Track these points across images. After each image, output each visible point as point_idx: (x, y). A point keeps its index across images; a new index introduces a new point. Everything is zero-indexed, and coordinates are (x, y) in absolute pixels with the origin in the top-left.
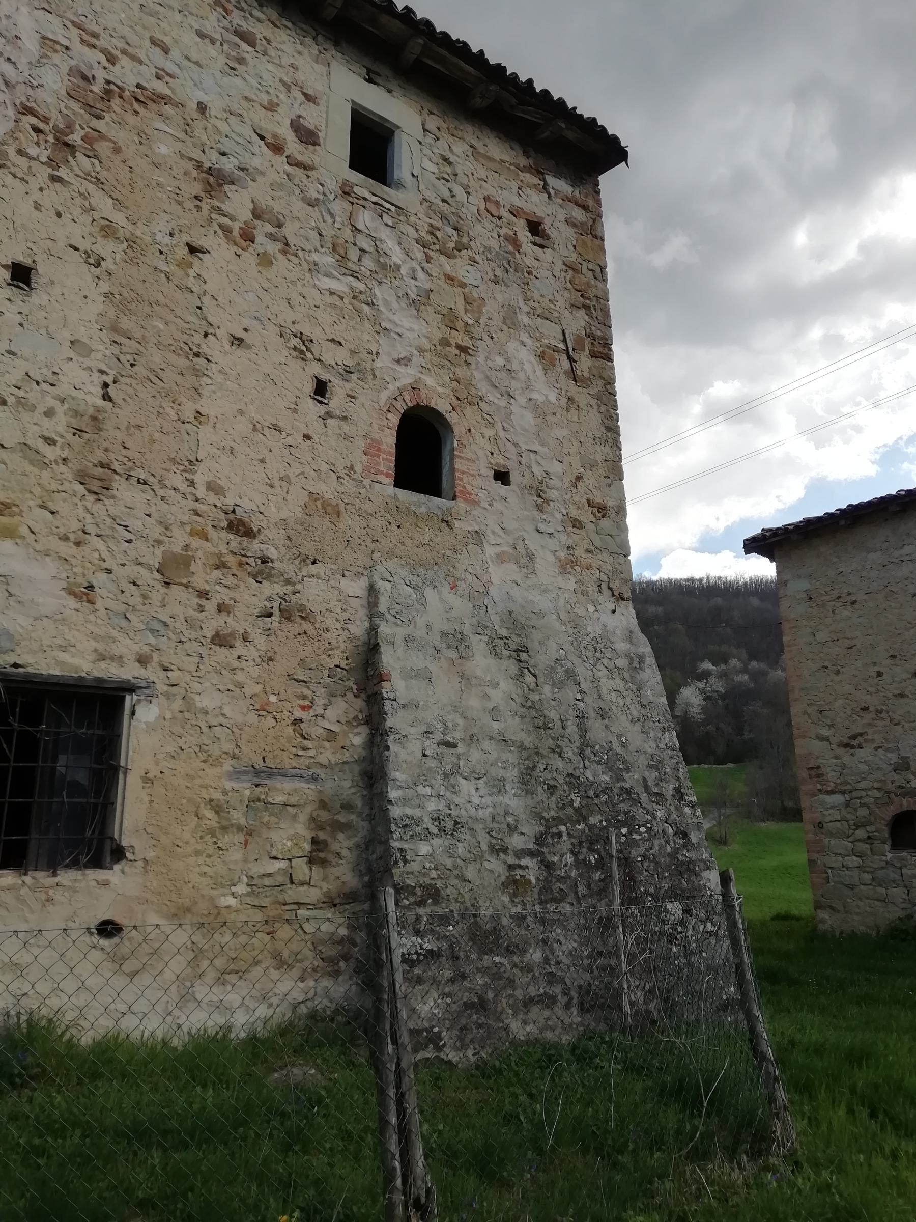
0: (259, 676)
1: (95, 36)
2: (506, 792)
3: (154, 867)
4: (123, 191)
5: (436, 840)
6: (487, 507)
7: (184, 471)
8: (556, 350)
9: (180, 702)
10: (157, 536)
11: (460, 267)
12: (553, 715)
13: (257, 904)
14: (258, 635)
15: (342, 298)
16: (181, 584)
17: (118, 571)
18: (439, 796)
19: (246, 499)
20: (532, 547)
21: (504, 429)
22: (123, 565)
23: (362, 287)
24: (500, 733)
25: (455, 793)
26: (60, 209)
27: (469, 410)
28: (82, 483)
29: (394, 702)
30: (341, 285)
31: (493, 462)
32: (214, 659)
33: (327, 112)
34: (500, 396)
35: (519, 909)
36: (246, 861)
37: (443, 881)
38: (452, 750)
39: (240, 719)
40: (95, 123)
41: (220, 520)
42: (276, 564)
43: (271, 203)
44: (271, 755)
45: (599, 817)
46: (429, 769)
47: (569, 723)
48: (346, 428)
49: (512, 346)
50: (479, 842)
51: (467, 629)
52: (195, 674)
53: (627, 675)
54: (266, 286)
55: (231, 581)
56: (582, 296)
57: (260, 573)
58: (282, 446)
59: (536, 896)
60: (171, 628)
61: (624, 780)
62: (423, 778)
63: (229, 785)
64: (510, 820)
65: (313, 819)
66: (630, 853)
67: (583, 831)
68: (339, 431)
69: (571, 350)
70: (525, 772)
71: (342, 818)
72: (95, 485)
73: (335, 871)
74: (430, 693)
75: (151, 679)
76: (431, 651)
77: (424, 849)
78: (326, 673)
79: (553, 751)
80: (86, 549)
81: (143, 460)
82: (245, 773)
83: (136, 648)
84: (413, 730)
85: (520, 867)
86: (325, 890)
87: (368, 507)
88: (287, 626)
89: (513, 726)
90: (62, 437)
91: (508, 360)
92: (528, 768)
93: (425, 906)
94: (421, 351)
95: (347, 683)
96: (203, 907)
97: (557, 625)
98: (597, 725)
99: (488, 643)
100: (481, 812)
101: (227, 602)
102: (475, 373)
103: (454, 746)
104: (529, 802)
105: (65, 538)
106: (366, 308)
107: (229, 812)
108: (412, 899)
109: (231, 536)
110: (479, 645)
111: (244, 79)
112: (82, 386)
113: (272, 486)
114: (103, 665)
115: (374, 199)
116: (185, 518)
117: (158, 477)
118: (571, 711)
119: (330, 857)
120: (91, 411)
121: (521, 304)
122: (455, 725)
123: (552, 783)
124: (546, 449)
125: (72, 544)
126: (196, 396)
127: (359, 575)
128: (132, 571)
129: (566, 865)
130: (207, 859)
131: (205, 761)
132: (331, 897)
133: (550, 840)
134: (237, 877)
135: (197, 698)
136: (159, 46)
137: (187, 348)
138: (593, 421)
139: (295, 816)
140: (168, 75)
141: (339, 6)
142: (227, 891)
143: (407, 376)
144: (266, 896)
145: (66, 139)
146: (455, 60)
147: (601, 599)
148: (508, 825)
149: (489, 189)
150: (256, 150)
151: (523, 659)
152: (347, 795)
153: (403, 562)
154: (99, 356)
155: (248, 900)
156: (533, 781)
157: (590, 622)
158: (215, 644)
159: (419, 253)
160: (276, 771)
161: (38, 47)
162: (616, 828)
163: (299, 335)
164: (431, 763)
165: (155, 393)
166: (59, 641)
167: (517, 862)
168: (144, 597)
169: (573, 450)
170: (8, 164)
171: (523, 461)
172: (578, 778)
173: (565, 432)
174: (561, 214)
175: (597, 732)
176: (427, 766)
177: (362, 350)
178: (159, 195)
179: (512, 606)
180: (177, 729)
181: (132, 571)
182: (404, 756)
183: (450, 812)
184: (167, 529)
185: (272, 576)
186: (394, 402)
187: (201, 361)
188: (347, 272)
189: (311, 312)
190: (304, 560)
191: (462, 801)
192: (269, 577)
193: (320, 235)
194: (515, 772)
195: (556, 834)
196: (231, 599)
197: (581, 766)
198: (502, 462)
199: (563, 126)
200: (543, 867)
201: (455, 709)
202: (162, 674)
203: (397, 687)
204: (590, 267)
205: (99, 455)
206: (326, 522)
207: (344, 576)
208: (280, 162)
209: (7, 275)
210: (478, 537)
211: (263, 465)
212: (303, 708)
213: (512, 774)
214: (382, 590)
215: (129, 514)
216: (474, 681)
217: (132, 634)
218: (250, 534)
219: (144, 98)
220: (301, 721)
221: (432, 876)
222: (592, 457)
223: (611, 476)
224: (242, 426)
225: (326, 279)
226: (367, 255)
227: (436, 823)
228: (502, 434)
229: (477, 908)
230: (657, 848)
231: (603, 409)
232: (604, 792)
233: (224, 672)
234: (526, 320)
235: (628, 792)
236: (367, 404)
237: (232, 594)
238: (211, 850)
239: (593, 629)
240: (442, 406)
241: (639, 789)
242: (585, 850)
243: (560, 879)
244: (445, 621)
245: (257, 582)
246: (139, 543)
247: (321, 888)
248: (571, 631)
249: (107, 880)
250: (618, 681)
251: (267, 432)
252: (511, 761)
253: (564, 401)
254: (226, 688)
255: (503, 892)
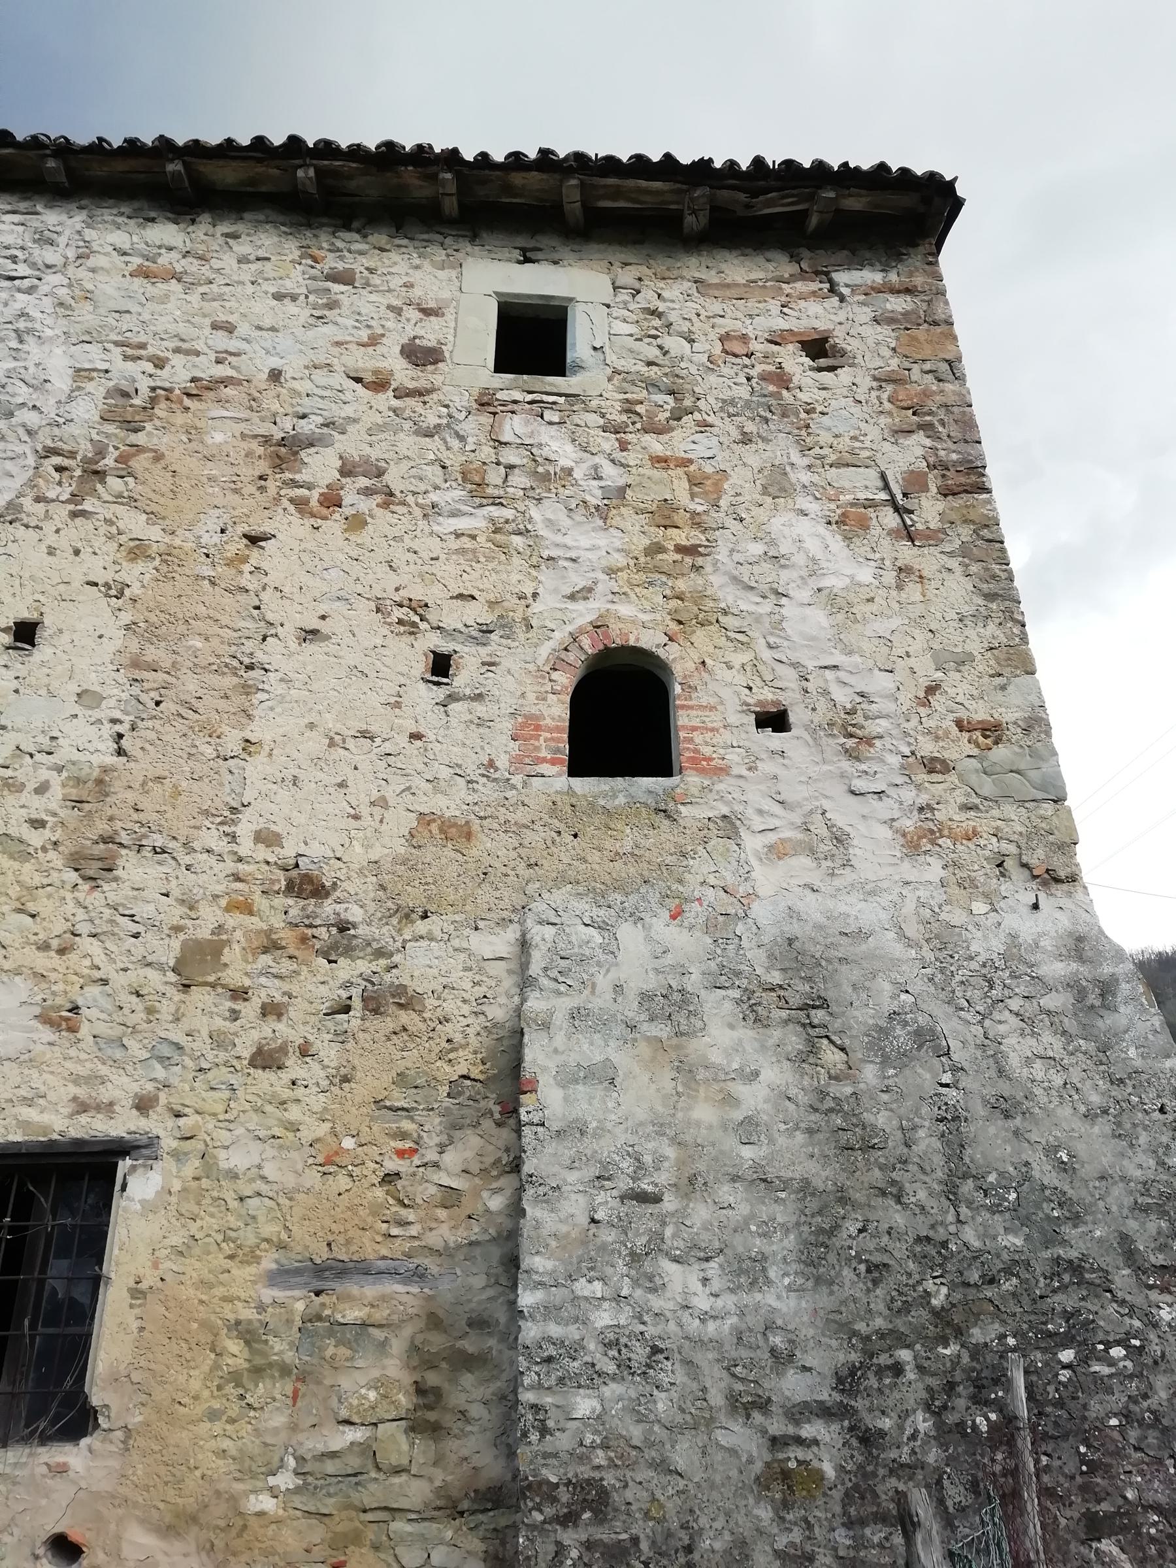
0: (325, 1109)
1: (142, 346)
2: (769, 1282)
3: (141, 1442)
4: (162, 501)
5: (613, 1386)
6: (745, 773)
7: (221, 823)
8: (871, 504)
9: (197, 1163)
10: (175, 921)
11: (683, 441)
12: (881, 1120)
13: (313, 1509)
14: (326, 1043)
15: (474, 537)
16: (206, 984)
17: (119, 981)
18: (618, 1298)
19: (315, 845)
20: (840, 820)
21: (770, 647)
22: (125, 970)
23: (508, 513)
24: (756, 1166)
25: (653, 1290)
26: (79, 545)
27: (700, 636)
28: (76, 870)
29: (540, 1129)
30: (477, 521)
31: (750, 701)
32: (253, 1089)
33: (456, 320)
34: (759, 600)
35: (796, 1535)
36: (294, 1428)
37: (620, 1473)
38: (651, 1208)
39: (290, 1181)
40: (134, 438)
41: (273, 882)
42: (362, 930)
43: (368, 450)
44: (341, 1239)
45: (996, 1328)
46: (603, 1248)
47: (921, 1133)
48: (480, 709)
49: (777, 524)
50: (704, 1390)
51: (694, 982)
52: (221, 1117)
53: (1070, 1024)
54: (354, 554)
55: (286, 966)
56: (914, 414)
57: (334, 947)
58: (375, 758)
59: (838, 1509)
60: (188, 1050)
61: (1064, 1243)
62: (589, 1264)
63: (268, 1294)
64: (777, 1340)
65: (414, 1349)
66: (1085, 1407)
67: (956, 1360)
68: (470, 717)
69: (899, 497)
70: (812, 1239)
71: (470, 1345)
72: (92, 869)
73: (455, 1447)
74: (611, 1105)
75: (155, 1132)
76: (618, 1030)
77: (585, 1405)
78: (444, 1090)
79: (883, 1193)
80: (73, 957)
81: (163, 822)
82: (297, 1272)
83: (135, 1088)
84: (572, 1177)
85: (800, 1441)
86: (438, 1483)
87: (521, 816)
88: (375, 1023)
89: (796, 1155)
90: (55, 814)
91: (773, 543)
92: (821, 1231)
93: (576, 1525)
94: (611, 572)
95: (483, 1104)
96: (218, 1513)
97: (899, 950)
98: (992, 1130)
99: (739, 1002)
100: (711, 1326)
101: (278, 998)
102: (712, 578)
103: (656, 1199)
104: (824, 1300)
105: (44, 947)
106: (517, 540)
107: (266, 1341)
108: (549, 1511)
109: (291, 901)
110: (718, 1010)
111: (336, 324)
112: (87, 746)
113: (356, 817)
114: (84, 1119)
115: (530, 397)
116: (219, 889)
117: (182, 839)
118: (925, 1110)
119: (448, 1420)
120: (96, 773)
121: (795, 457)
122: (659, 1160)
123: (877, 1258)
124: (856, 658)
125: (53, 954)
126: (244, 720)
127: (504, 922)
128: (137, 975)
129: (913, 1437)
130: (228, 1427)
131: (231, 1257)
132: (449, 1497)
133: (873, 1382)
134: (276, 1459)
135: (222, 1154)
136: (221, 328)
137: (235, 663)
138: (956, 591)
139: (383, 1345)
140: (231, 354)
141: (454, 191)
142: (260, 1484)
143: (584, 613)
144: (329, 1495)
145: (95, 467)
146: (631, 183)
147: (1005, 887)
148: (773, 1351)
149: (727, 325)
150: (348, 396)
151: (816, 1021)
152: (480, 1303)
153: (581, 889)
154: (112, 702)
155: (297, 1501)
156: (832, 1258)
157: (979, 934)
158: (255, 1067)
159: (608, 443)
160: (352, 1265)
161: (70, 382)
162: (1044, 1350)
163: (406, 602)
164: (608, 1236)
165: (185, 730)
166: (23, 1092)
167: (791, 1430)
168: (150, 1011)
169: (916, 647)
170: (23, 516)
171: (810, 686)
172: (944, 1244)
173: (895, 622)
174: (864, 314)
175: (991, 1144)
176: (598, 1241)
177: (508, 596)
178: (210, 490)
179: (795, 929)
180: (190, 1207)
181: (137, 975)
182: (555, 1220)
183: (642, 1328)
184: (191, 908)
185: (353, 949)
186: (563, 655)
187: (256, 674)
188: (485, 501)
189: (426, 568)
190: (407, 916)
191: (671, 1305)
192: (348, 951)
193: (444, 467)
194: (791, 1240)
195: (888, 1367)
196: (284, 993)
197: (951, 1218)
198: (770, 697)
199: (832, 195)
200: (855, 1443)
201: (661, 1128)
202: (171, 1122)
203: (549, 1100)
204: (927, 366)
205: (102, 827)
206: (448, 852)
207: (476, 929)
208: (386, 400)
209: (7, 639)
210: (729, 826)
211: (343, 791)
212: (401, 1154)
213: (784, 1245)
214: (537, 939)
215: (135, 898)
216: (701, 1074)
217: (129, 1068)
218: (319, 891)
219: (199, 389)
220: (397, 1175)
221: (597, 1461)
222: (959, 650)
223: (1006, 671)
224: (315, 743)
225: (452, 521)
226: (516, 471)
227: (614, 1353)
228: (766, 654)
229: (695, 1535)
230: (1163, 1395)
231: (974, 568)
232: (1008, 1272)
233: (269, 1108)
234: (805, 477)
235: (1075, 1268)
236: (515, 668)
237: (286, 987)
238: (234, 1409)
239: (985, 945)
240: (649, 640)
241: (1111, 1260)
242: (961, 1403)
243: (897, 1469)
244: (651, 974)
245: (330, 962)
246: (150, 938)
247: (431, 1480)
248: (930, 956)
249: (65, 1464)
250: (1047, 1037)
251: (350, 743)
252: (780, 1219)
253: (890, 577)
254: (269, 1133)
255: (758, 1501)
